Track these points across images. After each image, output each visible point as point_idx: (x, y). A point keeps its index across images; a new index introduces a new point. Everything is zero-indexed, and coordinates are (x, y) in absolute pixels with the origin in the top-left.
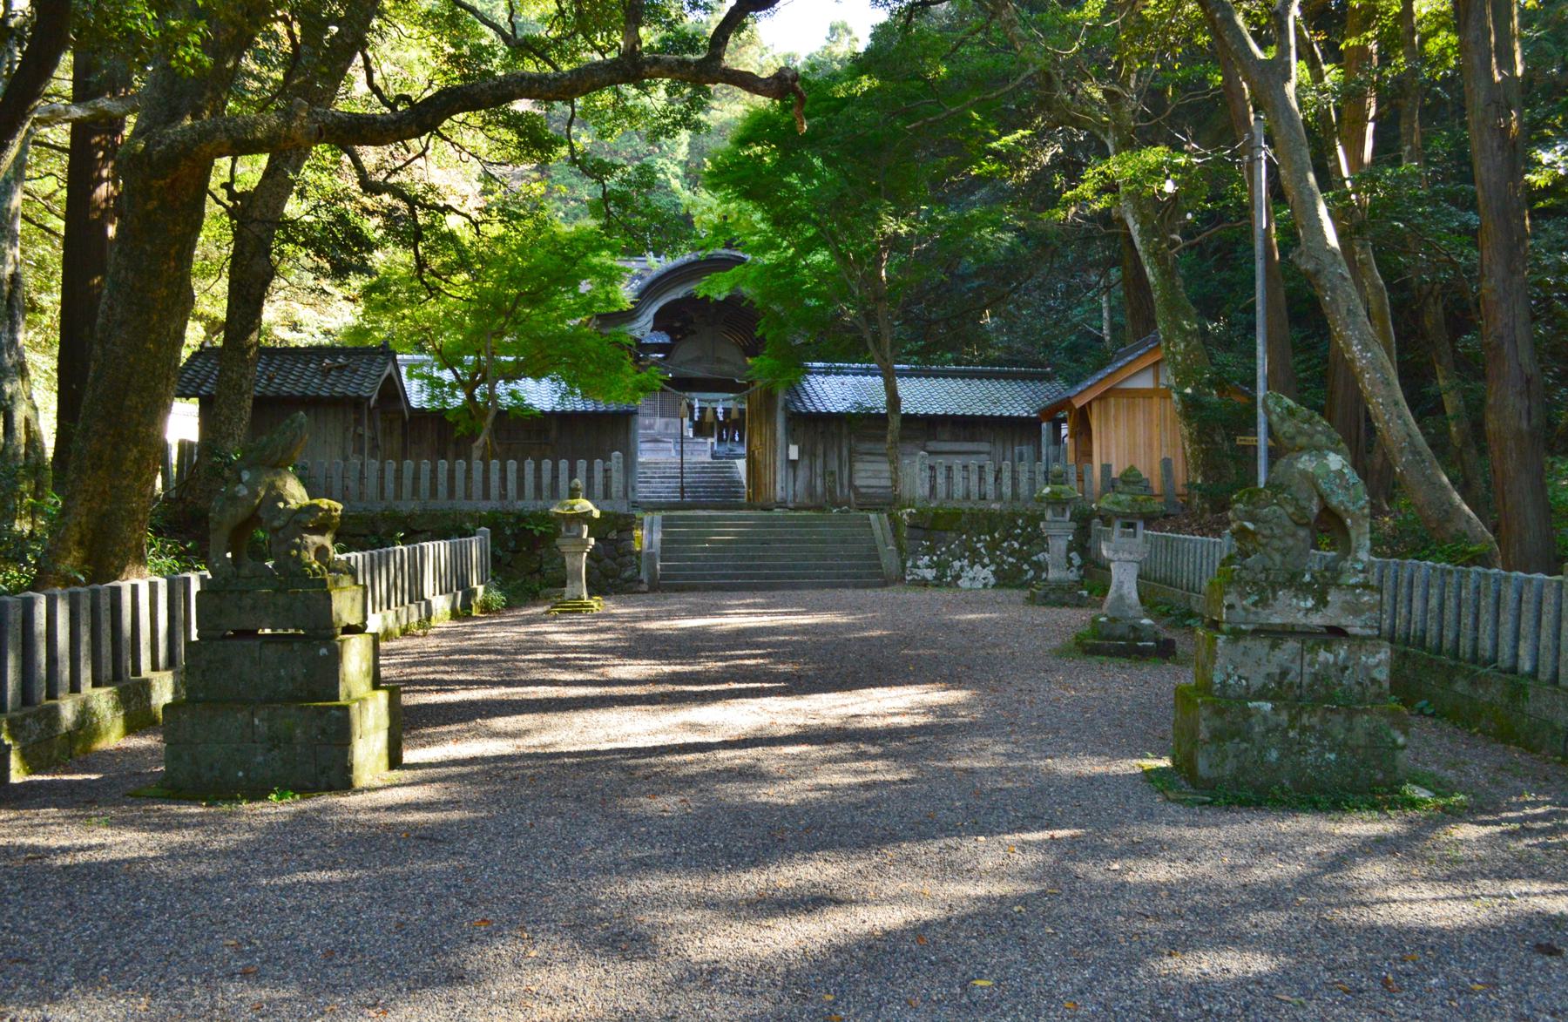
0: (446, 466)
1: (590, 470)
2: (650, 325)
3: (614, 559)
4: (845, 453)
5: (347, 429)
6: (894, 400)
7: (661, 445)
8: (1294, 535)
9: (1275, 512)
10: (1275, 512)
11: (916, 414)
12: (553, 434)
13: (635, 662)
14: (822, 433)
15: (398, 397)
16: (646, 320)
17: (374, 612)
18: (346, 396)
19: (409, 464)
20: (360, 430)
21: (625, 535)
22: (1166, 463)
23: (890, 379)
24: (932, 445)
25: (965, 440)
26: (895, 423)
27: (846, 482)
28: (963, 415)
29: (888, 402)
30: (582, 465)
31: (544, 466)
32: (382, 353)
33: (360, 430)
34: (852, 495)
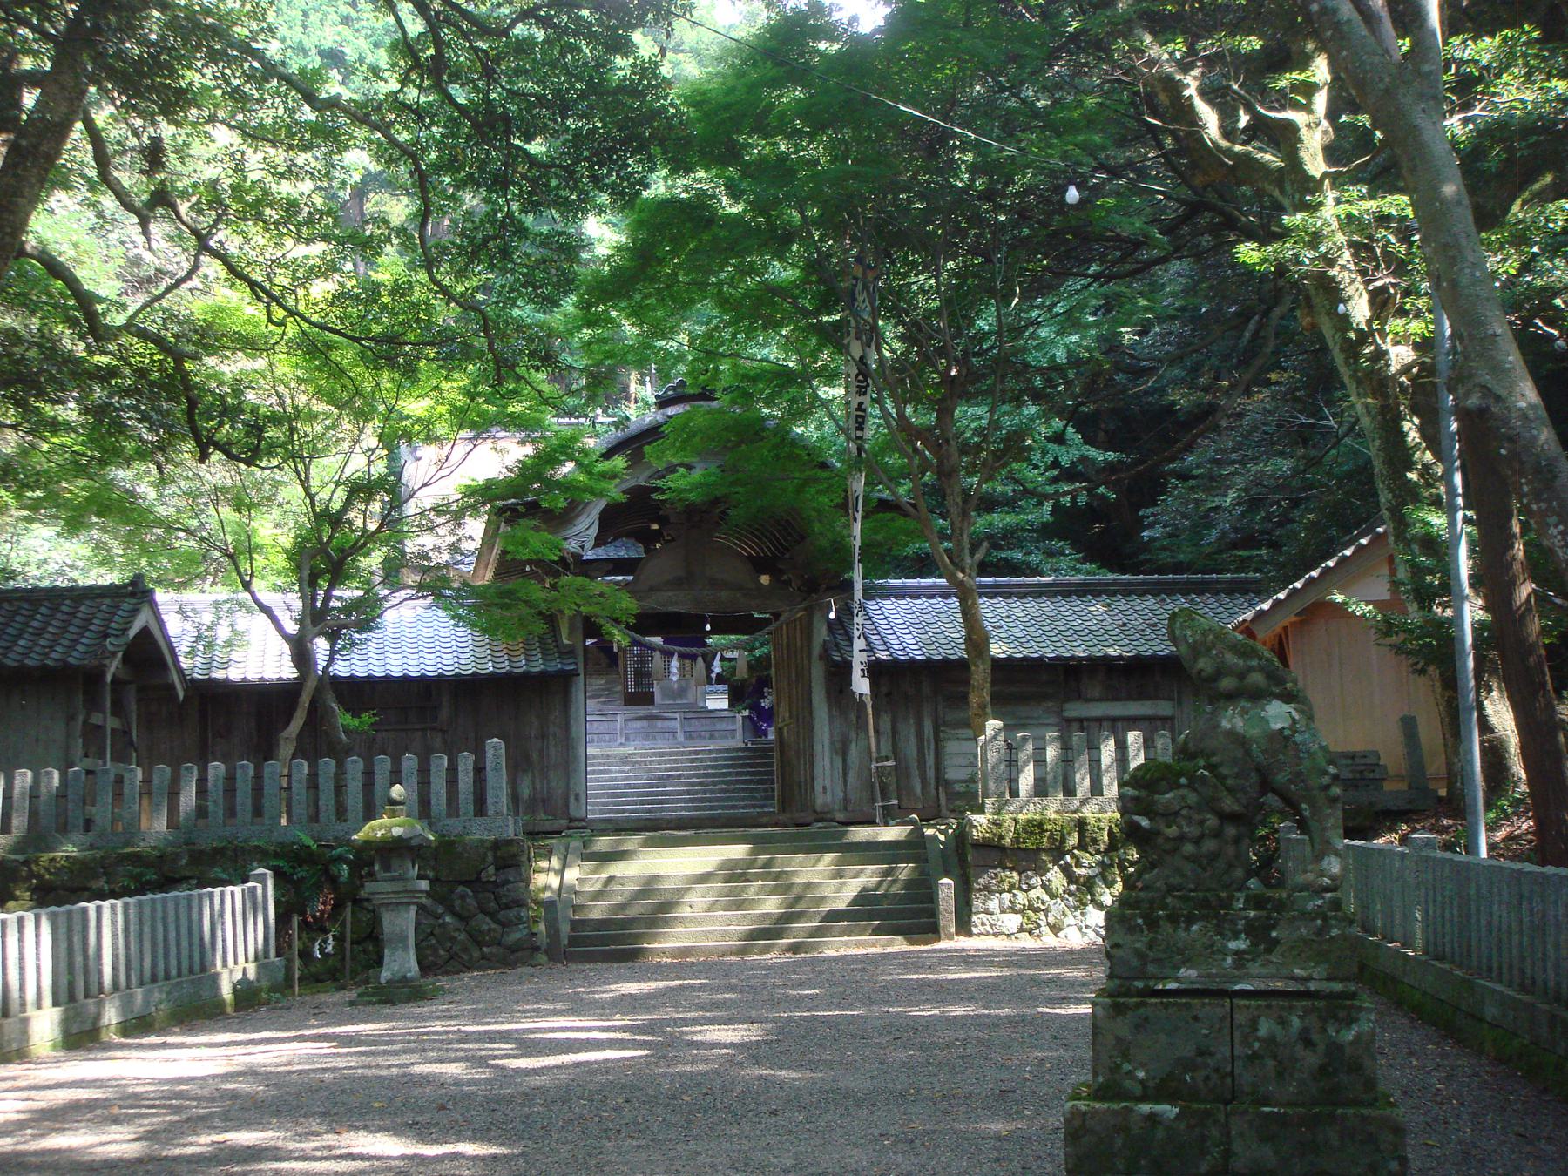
0: (251, 772)
1: (424, 771)
2: (594, 531)
3: (492, 915)
4: (928, 725)
5: (71, 718)
6: (976, 638)
7: (659, 724)
8: (1217, 834)
9: (1183, 797)
10: (1183, 797)
11: (1041, 658)
12: (445, 713)
13: (190, 1040)
14: (888, 694)
15: (165, 666)
16: (588, 522)
17: (39, 1006)
18: (67, 666)
19: (217, 768)
20: (96, 719)
21: (511, 875)
22: (1409, 726)
23: (966, 597)
24: (1075, 710)
25: (1130, 697)
26: (980, 675)
27: (931, 774)
28: (1025, 658)
29: (969, 640)
30: (410, 762)
31: (211, 772)
32: (133, 595)
33: (96, 719)
34: (942, 796)
